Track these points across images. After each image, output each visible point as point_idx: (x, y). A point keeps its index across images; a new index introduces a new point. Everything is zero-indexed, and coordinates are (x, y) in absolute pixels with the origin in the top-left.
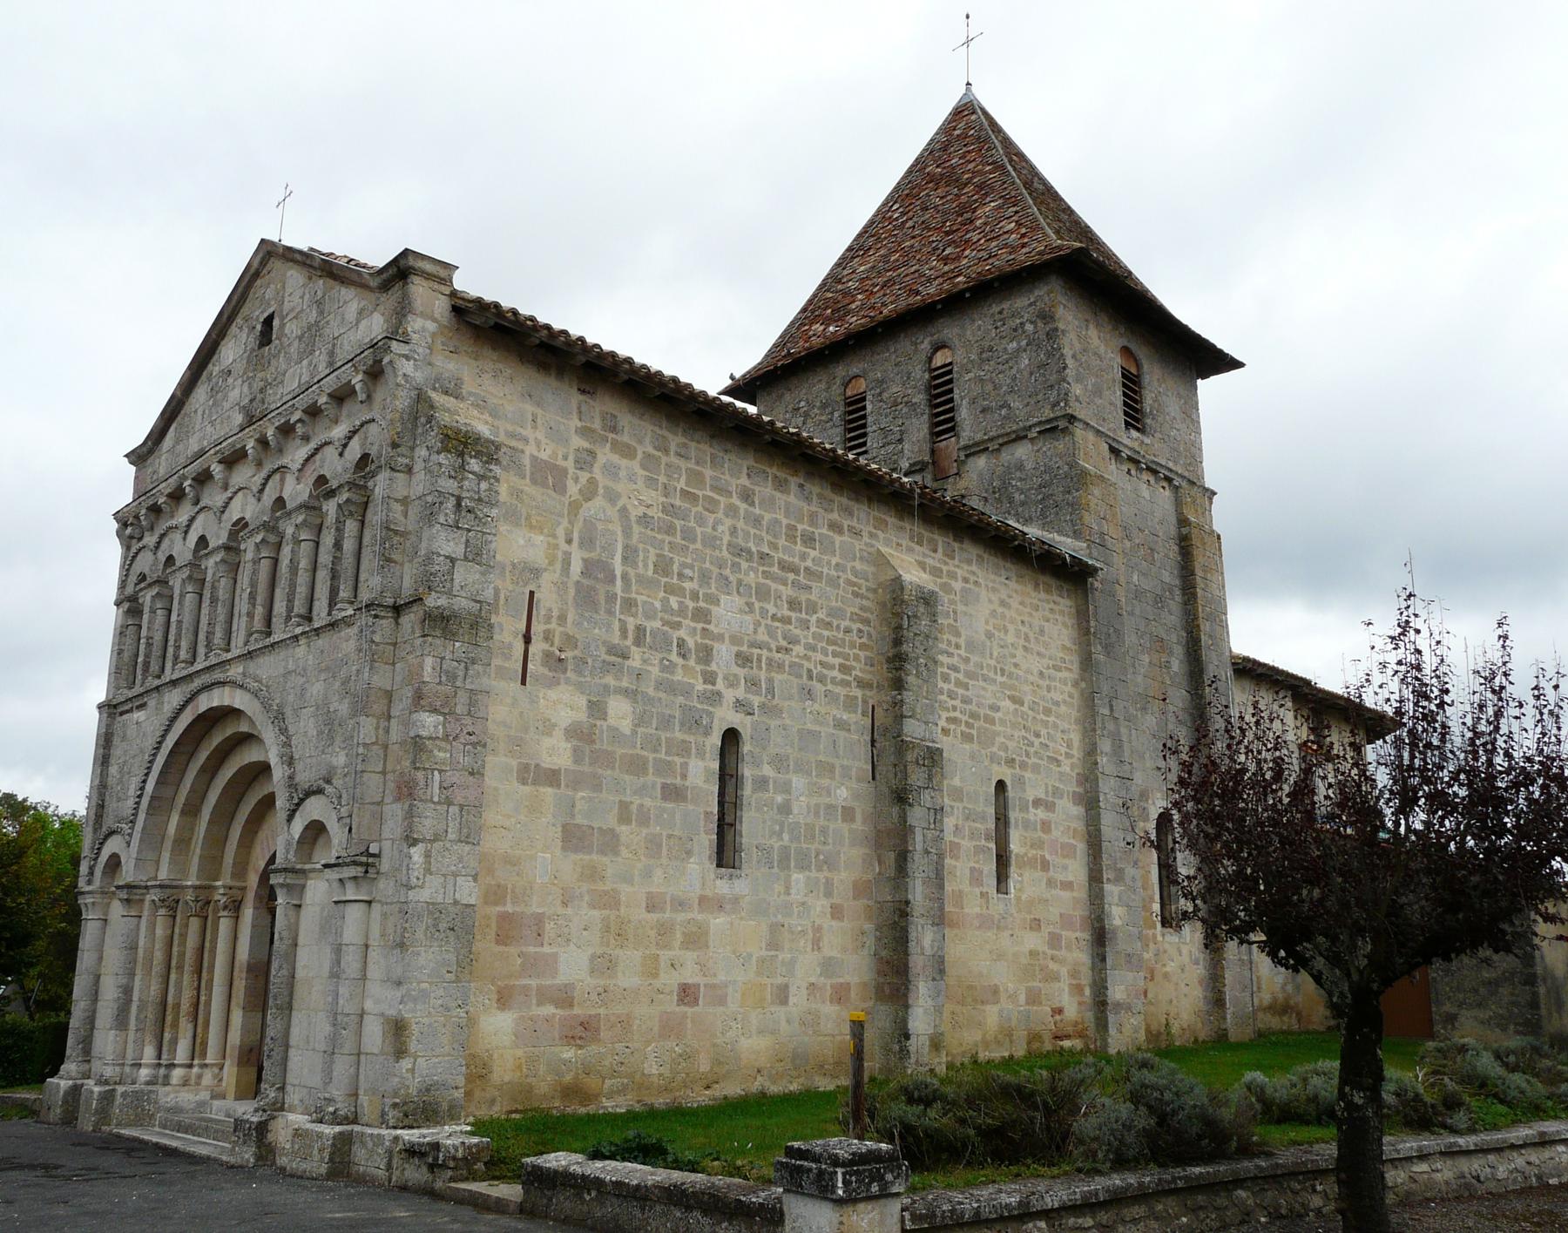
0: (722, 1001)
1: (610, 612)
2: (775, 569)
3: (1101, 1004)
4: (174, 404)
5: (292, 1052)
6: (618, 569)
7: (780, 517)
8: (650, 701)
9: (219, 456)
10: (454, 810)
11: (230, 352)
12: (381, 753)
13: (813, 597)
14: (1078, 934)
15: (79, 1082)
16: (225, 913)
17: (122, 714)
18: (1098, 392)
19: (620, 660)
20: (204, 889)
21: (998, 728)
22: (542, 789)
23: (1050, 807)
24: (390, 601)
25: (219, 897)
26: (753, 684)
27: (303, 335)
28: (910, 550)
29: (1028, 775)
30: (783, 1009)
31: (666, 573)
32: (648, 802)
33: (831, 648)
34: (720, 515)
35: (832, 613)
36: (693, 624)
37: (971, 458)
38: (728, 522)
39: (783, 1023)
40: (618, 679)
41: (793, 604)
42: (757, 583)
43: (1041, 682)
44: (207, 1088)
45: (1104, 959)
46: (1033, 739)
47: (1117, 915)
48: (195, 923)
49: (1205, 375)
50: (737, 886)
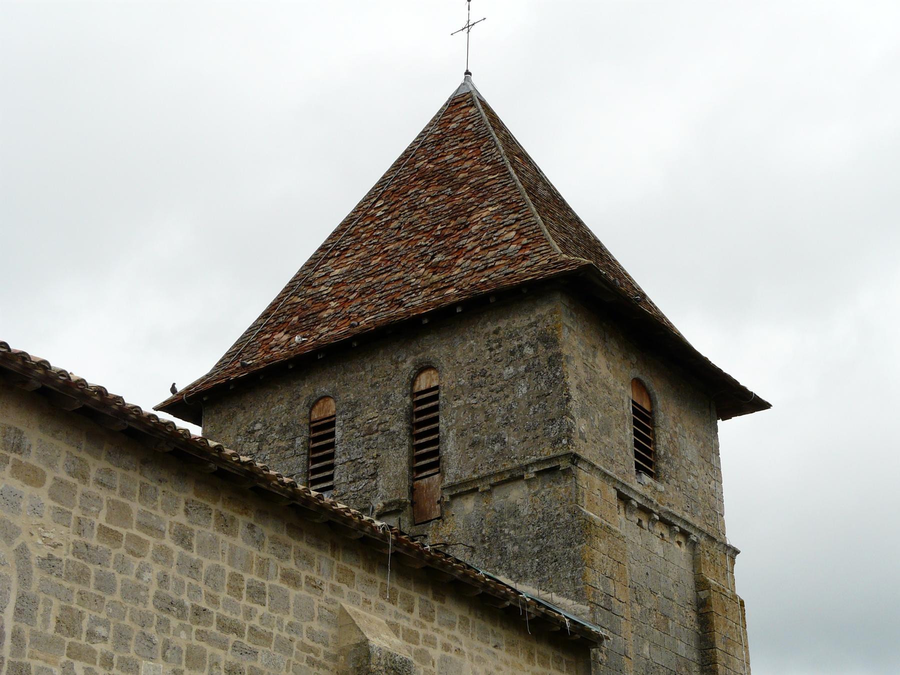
2: (213, 628)
18: (606, 429)
31: (72, 631)
34: (148, 559)
38: (157, 569)
42: (190, 647)
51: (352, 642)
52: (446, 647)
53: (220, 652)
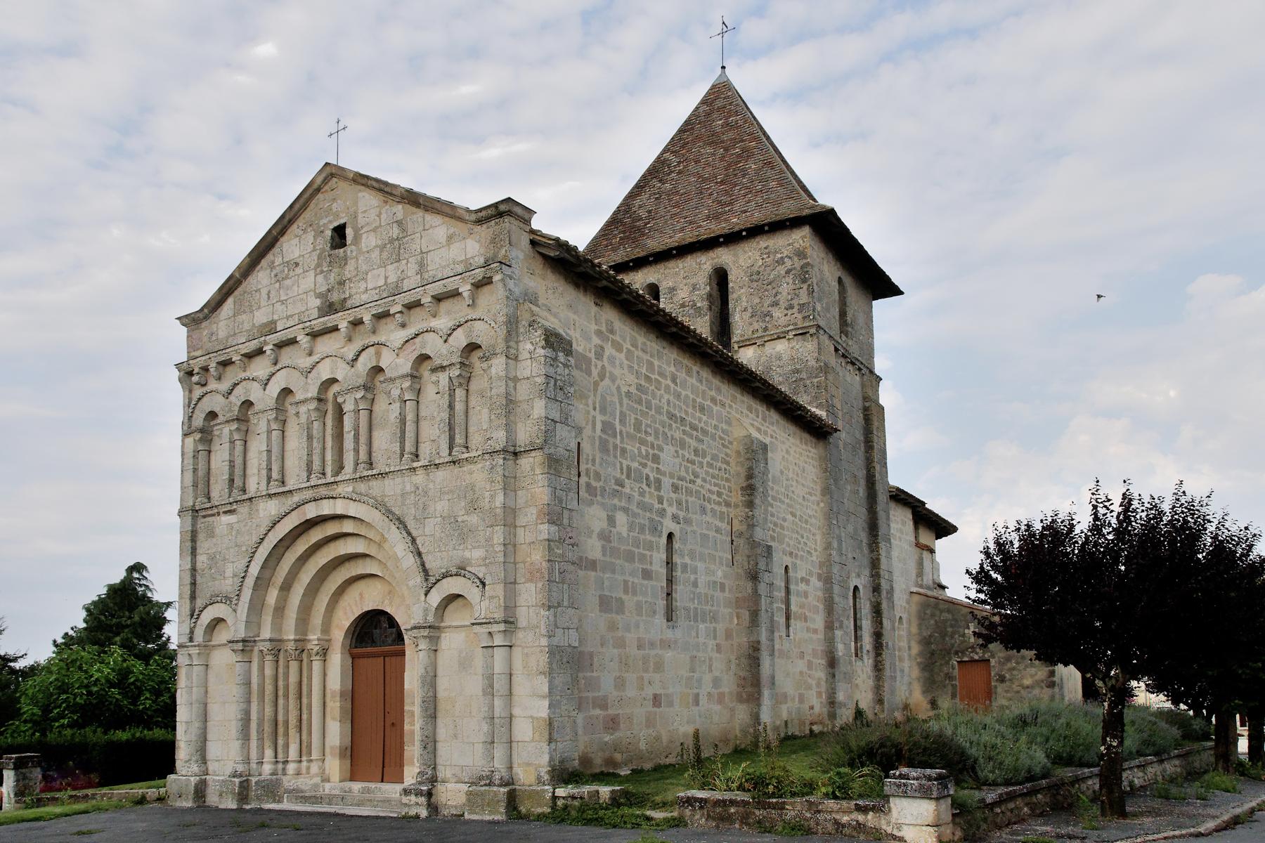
0: (671, 704)
1: (615, 457)
2: (687, 429)
3: (832, 703)
4: (231, 282)
5: (439, 745)
6: (618, 427)
7: (689, 394)
8: (635, 515)
9: (308, 330)
10: (566, 586)
11: (293, 247)
12: (512, 549)
13: (704, 447)
14: (820, 661)
15: (204, 777)
16: (318, 658)
17: (204, 517)
18: (828, 310)
19: (620, 488)
20: (301, 642)
21: (786, 533)
22: (589, 573)
23: (807, 582)
24: (512, 449)
25: (312, 647)
26: (679, 503)
27: (384, 246)
28: (747, 416)
29: (798, 562)
30: (697, 708)
31: (639, 431)
32: (636, 581)
33: (713, 480)
34: (662, 392)
35: (714, 457)
36: (653, 465)
37: (742, 349)
38: (666, 397)
39: (698, 717)
40: (620, 501)
41: (696, 451)
42: (680, 438)
43: (803, 503)
44: (317, 775)
45: (834, 676)
46: (800, 539)
47: (840, 649)
48: (294, 666)
49: (877, 297)
50: (678, 634)
51: (741, 435)
52: (772, 437)
53: (691, 441)
